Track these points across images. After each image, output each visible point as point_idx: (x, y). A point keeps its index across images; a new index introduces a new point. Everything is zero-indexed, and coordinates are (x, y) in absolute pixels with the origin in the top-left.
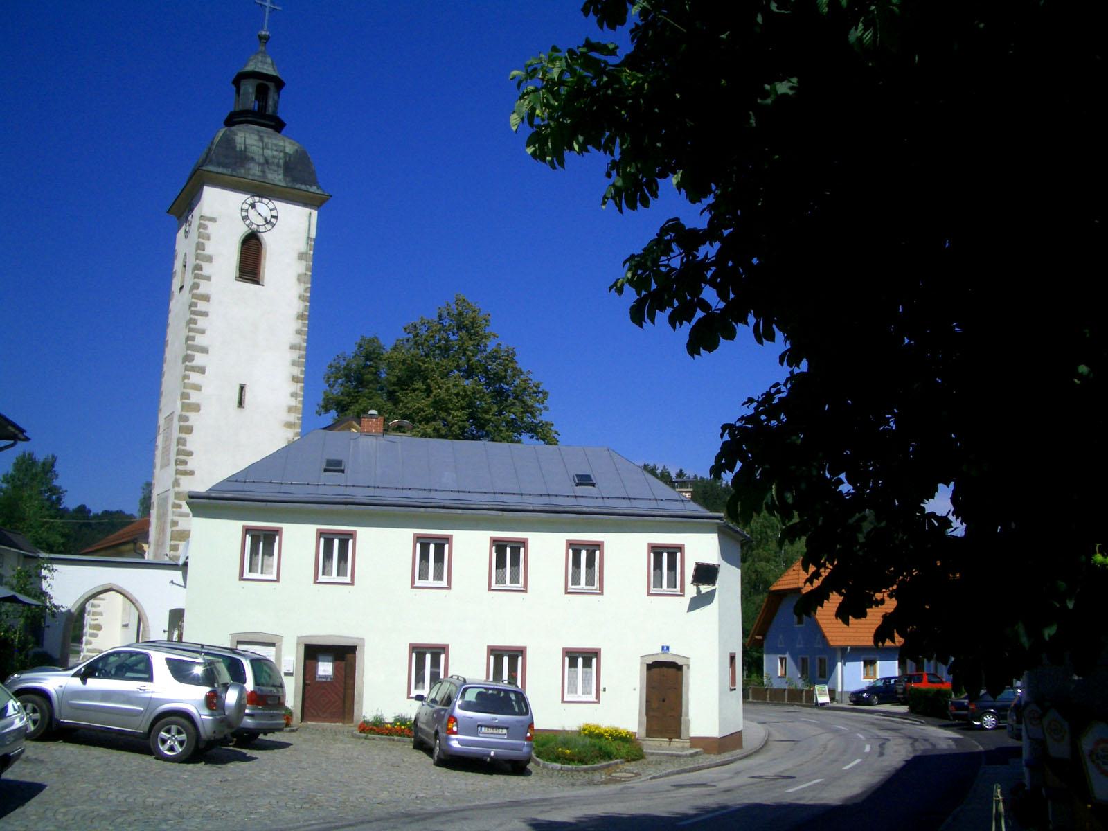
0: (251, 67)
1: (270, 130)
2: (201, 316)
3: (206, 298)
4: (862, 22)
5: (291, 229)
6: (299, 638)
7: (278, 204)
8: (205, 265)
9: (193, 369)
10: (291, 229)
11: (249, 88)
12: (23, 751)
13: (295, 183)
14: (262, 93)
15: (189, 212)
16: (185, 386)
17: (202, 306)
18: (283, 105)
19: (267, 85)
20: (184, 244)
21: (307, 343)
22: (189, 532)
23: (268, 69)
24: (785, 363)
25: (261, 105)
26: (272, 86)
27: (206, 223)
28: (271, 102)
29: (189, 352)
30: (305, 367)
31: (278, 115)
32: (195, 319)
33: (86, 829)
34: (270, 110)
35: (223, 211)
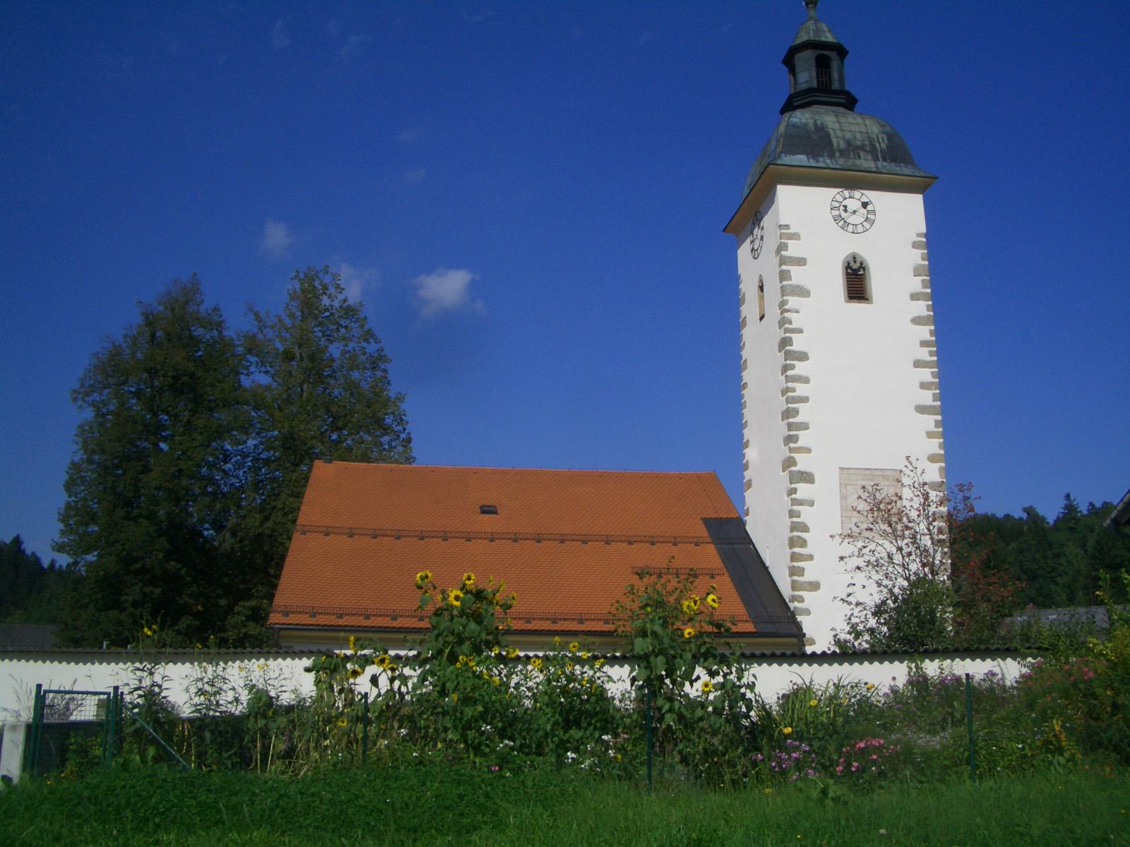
0: (803, 38)
1: (842, 109)
2: (803, 402)
3: (803, 357)
4: (919, 682)
5: (894, 226)
6: (1031, 507)
7: (871, 195)
8: (794, 270)
9: (801, 503)
10: (894, 226)
11: (806, 61)
12: (193, 712)
13: (890, 165)
14: (823, 64)
15: (754, 224)
16: (783, 261)
17: (800, 389)
18: (851, 76)
19: (827, 56)
20: (752, 265)
21: (933, 311)
22: (853, 110)
23: (829, 37)
24: (964, 677)
25: (823, 77)
26: (832, 54)
27: (795, 455)
28: (835, 75)
29: (784, 267)
30: (937, 356)
31: (847, 89)
32: (794, 409)
33: (598, 845)
34: (836, 86)
35: (800, 208)
